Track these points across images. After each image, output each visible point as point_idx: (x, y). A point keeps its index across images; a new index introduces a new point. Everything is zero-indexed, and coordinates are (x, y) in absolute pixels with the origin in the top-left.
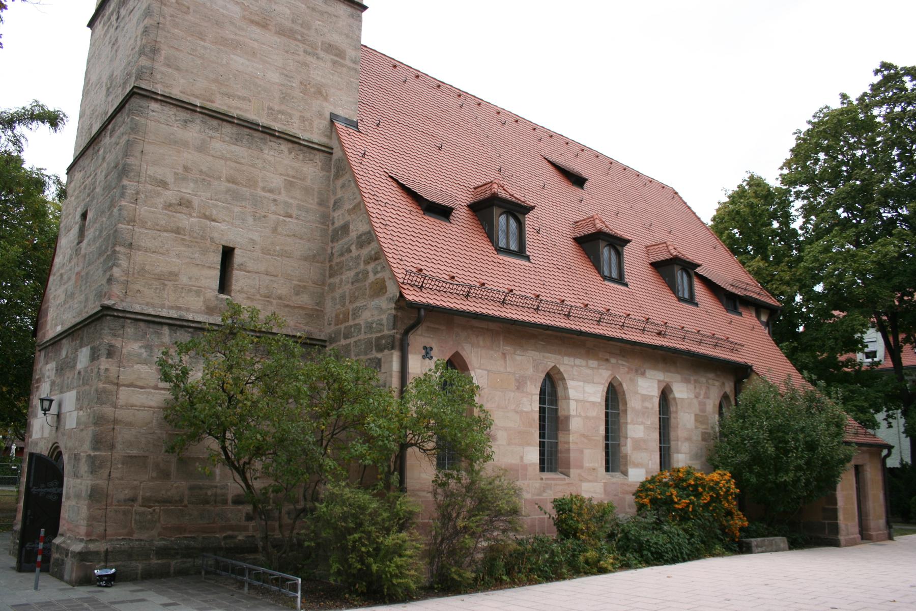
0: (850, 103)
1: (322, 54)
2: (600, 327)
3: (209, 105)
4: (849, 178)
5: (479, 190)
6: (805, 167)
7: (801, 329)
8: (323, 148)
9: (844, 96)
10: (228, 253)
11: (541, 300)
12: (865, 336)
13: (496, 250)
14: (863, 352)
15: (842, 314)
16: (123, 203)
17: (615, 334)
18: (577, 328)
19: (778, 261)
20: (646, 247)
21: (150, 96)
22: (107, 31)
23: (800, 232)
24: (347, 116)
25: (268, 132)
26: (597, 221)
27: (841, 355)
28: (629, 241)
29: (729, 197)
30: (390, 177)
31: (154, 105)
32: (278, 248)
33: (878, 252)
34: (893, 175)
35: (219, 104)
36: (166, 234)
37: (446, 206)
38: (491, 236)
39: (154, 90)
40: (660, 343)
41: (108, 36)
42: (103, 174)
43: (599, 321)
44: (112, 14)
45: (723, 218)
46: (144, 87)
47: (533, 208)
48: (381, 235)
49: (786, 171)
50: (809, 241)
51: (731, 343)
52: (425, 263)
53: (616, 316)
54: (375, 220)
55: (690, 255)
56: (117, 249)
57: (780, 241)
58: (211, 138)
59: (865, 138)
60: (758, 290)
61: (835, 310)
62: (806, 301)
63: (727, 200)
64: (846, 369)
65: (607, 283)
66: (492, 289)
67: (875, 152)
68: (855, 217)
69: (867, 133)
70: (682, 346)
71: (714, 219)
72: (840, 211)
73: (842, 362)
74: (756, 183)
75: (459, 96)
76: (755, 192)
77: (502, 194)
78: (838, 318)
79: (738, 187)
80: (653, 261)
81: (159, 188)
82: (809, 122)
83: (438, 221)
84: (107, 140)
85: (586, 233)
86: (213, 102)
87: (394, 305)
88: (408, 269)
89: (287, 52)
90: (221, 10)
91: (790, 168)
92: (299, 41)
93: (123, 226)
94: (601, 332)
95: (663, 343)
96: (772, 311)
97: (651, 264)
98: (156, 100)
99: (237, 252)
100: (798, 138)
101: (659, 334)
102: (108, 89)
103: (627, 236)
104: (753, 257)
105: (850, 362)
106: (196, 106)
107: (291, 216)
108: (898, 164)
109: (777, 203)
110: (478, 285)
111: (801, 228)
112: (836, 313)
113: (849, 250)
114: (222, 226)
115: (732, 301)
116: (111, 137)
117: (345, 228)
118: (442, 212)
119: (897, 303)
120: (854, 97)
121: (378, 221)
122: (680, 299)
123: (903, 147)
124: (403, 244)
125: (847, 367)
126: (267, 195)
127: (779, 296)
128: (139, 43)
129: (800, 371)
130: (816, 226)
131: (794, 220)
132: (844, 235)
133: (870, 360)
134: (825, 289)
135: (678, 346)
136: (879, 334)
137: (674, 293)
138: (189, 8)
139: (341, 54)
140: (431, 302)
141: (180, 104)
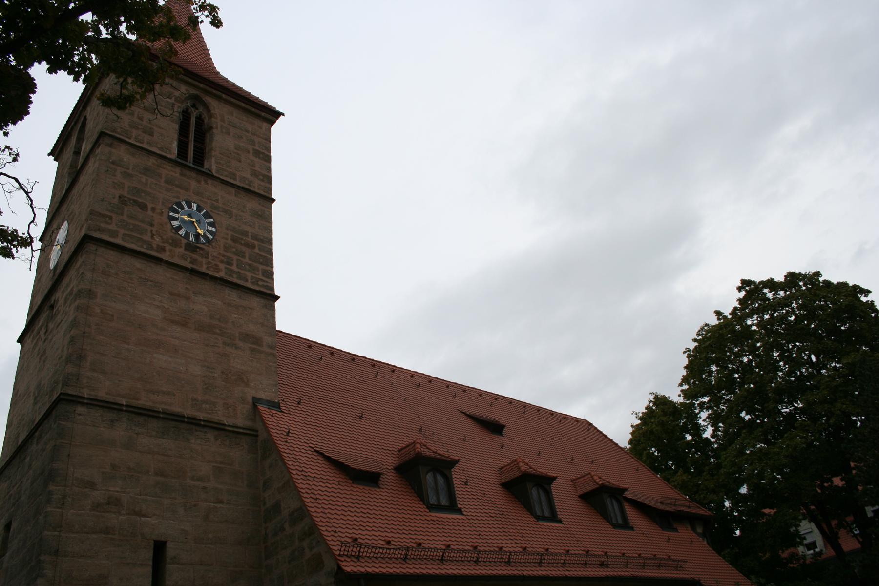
0: (725, 317)
1: (240, 344)
2: (542, 569)
3: (134, 403)
4: (742, 384)
5: (403, 451)
6: (701, 380)
7: (738, 532)
8: (248, 432)
9: (718, 313)
10: (159, 548)
11: (480, 551)
12: (800, 529)
13: (428, 508)
14: (803, 545)
15: (772, 511)
16: (49, 509)
17: (558, 573)
18: (520, 573)
19: (699, 472)
20: (572, 481)
21: (77, 400)
22: (36, 344)
23: (712, 440)
24: (269, 398)
25: (194, 422)
26: (521, 464)
27: (783, 552)
28: (554, 478)
29: (640, 419)
30: (316, 451)
31: (80, 409)
32: (211, 536)
33: (788, 446)
34: (780, 374)
35: (145, 401)
36: (94, 536)
37: (373, 472)
38: (421, 496)
39: (80, 394)
40: (604, 573)
41: (37, 349)
42: (29, 481)
43: (540, 562)
44: (41, 328)
45: (639, 441)
46: (70, 392)
47: (457, 461)
48: (313, 510)
49: (685, 387)
50: (722, 448)
51: (674, 560)
52: (360, 531)
53: (556, 554)
54: (305, 495)
55: (615, 481)
56: (42, 558)
57: (696, 452)
58: (138, 434)
59: (747, 346)
60: (687, 503)
61: (765, 508)
62: (735, 505)
63: (639, 422)
64: (791, 565)
65: (541, 523)
66: (429, 548)
67: (758, 356)
68: (758, 417)
69: (747, 340)
70: (626, 573)
71: (630, 442)
72: (743, 414)
73: (786, 558)
74: (660, 401)
75: (374, 366)
76: (663, 411)
77: (427, 452)
78: (769, 515)
79: (646, 408)
80: (581, 493)
81: (86, 490)
82: (695, 340)
83: (367, 488)
84: (34, 448)
85: (512, 477)
86: (137, 399)
87: (333, 580)
88: (343, 540)
89: (207, 345)
90: (143, 315)
91: (689, 384)
92: (218, 334)
93: (49, 533)
94: (544, 573)
95: (608, 573)
96: (705, 521)
97: (581, 496)
98: (83, 404)
99: (170, 545)
100: (689, 356)
101: (602, 565)
102: (36, 398)
103: (552, 474)
104: (676, 472)
105: (794, 557)
106: (122, 405)
107: (221, 502)
108: (781, 363)
109: (685, 417)
110: (414, 545)
111: (712, 436)
112: (767, 511)
113: (761, 449)
114: (153, 521)
115: (664, 519)
116: (37, 444)
117: (277, 508)
118: (370, 479)
119: (819, 491)
120: (727, 312)
121: (308, 496)
122: (616, 526)
123: (780, 348)
124: (335, 516)
125: (792, 563)
126: (198, 483)
127: (708, 504)
128: (65, 352)
129: (747, 576)
130: (725, 432)
131: (705, 430)
132: (753, 436)
133: (811, 552)
134: (748, 489)
135: (623, 574)
136: (812, 524)
137: (608, 521)
138: (112, 316)
139: (258, 341)
140: (370, 570)
141: (106, 405)
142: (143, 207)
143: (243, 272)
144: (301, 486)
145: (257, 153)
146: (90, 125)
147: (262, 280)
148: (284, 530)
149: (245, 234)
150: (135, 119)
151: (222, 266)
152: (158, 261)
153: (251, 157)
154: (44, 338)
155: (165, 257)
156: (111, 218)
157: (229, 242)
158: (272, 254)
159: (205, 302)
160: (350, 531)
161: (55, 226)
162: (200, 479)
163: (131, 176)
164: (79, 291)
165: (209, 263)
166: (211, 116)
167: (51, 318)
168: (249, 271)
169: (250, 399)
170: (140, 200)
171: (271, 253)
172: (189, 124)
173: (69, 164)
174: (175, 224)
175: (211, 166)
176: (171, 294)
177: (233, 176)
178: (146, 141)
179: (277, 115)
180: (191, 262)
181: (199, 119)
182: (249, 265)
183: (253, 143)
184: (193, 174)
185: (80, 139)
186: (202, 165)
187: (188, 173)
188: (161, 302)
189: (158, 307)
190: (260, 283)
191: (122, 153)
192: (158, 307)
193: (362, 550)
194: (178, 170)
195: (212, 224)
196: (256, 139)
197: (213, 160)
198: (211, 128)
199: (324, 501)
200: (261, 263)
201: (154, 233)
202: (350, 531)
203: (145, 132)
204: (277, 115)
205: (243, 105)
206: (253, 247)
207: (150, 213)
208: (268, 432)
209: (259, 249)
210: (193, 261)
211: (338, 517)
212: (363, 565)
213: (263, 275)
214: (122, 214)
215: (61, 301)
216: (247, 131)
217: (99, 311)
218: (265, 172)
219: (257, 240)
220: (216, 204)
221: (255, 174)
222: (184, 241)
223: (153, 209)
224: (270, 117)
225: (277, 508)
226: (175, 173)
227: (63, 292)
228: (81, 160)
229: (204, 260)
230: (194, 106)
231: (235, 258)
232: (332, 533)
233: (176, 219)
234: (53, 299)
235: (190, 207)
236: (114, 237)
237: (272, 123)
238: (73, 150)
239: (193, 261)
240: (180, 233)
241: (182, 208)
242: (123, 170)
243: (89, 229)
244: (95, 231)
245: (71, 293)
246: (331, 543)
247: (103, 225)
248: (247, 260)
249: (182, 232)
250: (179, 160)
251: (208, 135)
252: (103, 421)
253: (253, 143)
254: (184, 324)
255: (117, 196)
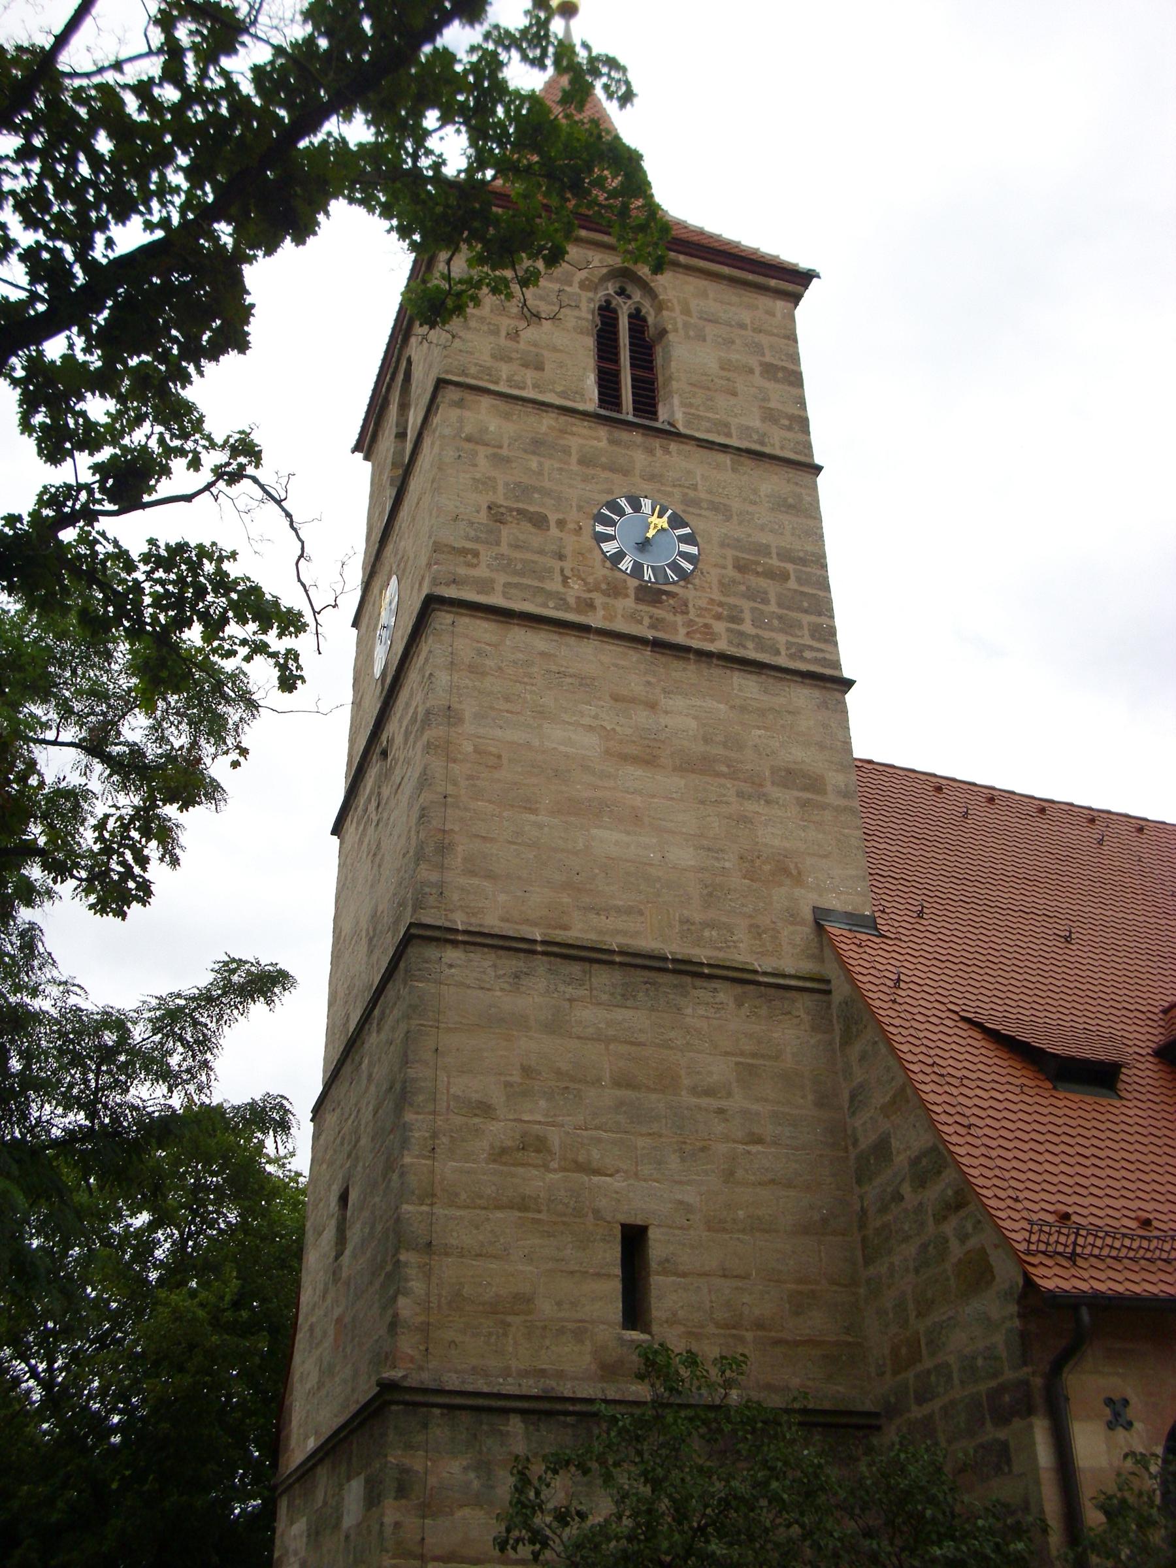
1: (775, 792)
10: (634, 1240)
21: (444, 936)
24: (849, 909)
25: (688, 970)
30: (964, 1019)
31: (452, 955)
35: (580, 931)
36: (499, 1215)
39: (448, 924)
42: (371, 1108)
44: (369, 800)
54: (944, 1118)
56: (403, 1257)
75: (1092, 821)
81: (476, 1120)
84: (373, 1040)
86: (566, 928)
87: (1013, 1308)
88: (1035, 1217)
89: (702, 802)
90: (562, 748)
92: (723, 775)
93: (410, 1208)
98: (455, 943)
99: (653, 1234)
102: (371, 940)
106: (535, 941)
107: (759, 1141)
114: (616, 1183)
118: (1100, 1076)
121: (950, 1120)
124: (1015, 1163)
126: (704, 1101)
128: (414, 842)
138: (499, 757)
139: (815, 784)
140: (1102, 1287)
141: (501, 943)
142: (539, 522)
143: (766, 634)
144: (931, 1098)
145: (769, 370)
146: (417, 373)
147: (811, 648)
148: (902, 1198)
149: (764, 550)
150: (502, 341)
151: (719, 627)
152: (583, 630)
153: (757, 379)
154: (375, 819)
155: (595, 620)
156: (476, 554)
157: (731, 572)
158: (827, 588)
159: (689, 708)
160: (1053, 1199)
161: (375, 590)
162: (709, 1092)
163: (507, 460)
164: (428, 713)
165: (690, 623)
166: (660, 307)
167: (386, 775)
168: (781, 630)
169: (808, 915)
170: (532, 509)
171: (824, 585)
172: (616, 333)
173: (389, 461)
174: (610, 548)
175: (673, 413)
176: (616, 698)
177: (725, 428)
178: (529, 382)
179: (805, 278)
180: (652, 626)
181: (637, 320)
182: (780, 618)
183: (759, 349)
184: (636, 437)
185: (404, 407)
186: (653, 414)
187: (624, 436)
188: (596, 717)
189: (591, 728)
190: (808, 654)
191: (483, 415)
192: (591, 728)
193: (1081, 1241)
194: (603, 432)
195: (689, 539)
196: (764, 339)
197: (676, 401)
198: (663, 333)
199: (987, 1131)
200: (806, 611)
201: (568, 573)
202: (1053, 1199)
203: (526, 365)
204: (805, 278)
205: (726, 270)
206: (785, 577)
207: (554, 531)
208: (852, 981)
209: (799, 580)
210: (655, 624)
211: (1023, 1167)
212: (1086, 1275)
213: (813, 637)
214: (498, 543)
215: (399, 740)
216: (742, 326)
217: (470, 749)
218: (793, 410)
219: (792, 561)
220: (691, 494)
221: (770, 416)
222: (633, 583)
223: (561, 523)
224: (790, 287)
225: (882, 1149)
226: (598, 438)
227: (400, 721)
228: (409, 446)
229: (679, 619)
230: (622, 292)
231: (746, 605)
232: (1010, 1202)
233: (611, 538)
234: (384, 738)
235: (637, 508)
236: (487, 594)
237: (796, 298)
238: (394, 431)
239: (655, 624)
240: (623, 566)
241: (621, 512)
242: (490, 451)
243: (435, 582)
244: (447, 585)
245: (414, 720)
246: (1007, 1224)
247: (462, 571)
248: (773, 608)
249: (626, 564)
250: (603, 412)
251: (659, 350)
252: (498, 977)
253: (759, 349)
254: (649, 761)
255: (485, 506)
